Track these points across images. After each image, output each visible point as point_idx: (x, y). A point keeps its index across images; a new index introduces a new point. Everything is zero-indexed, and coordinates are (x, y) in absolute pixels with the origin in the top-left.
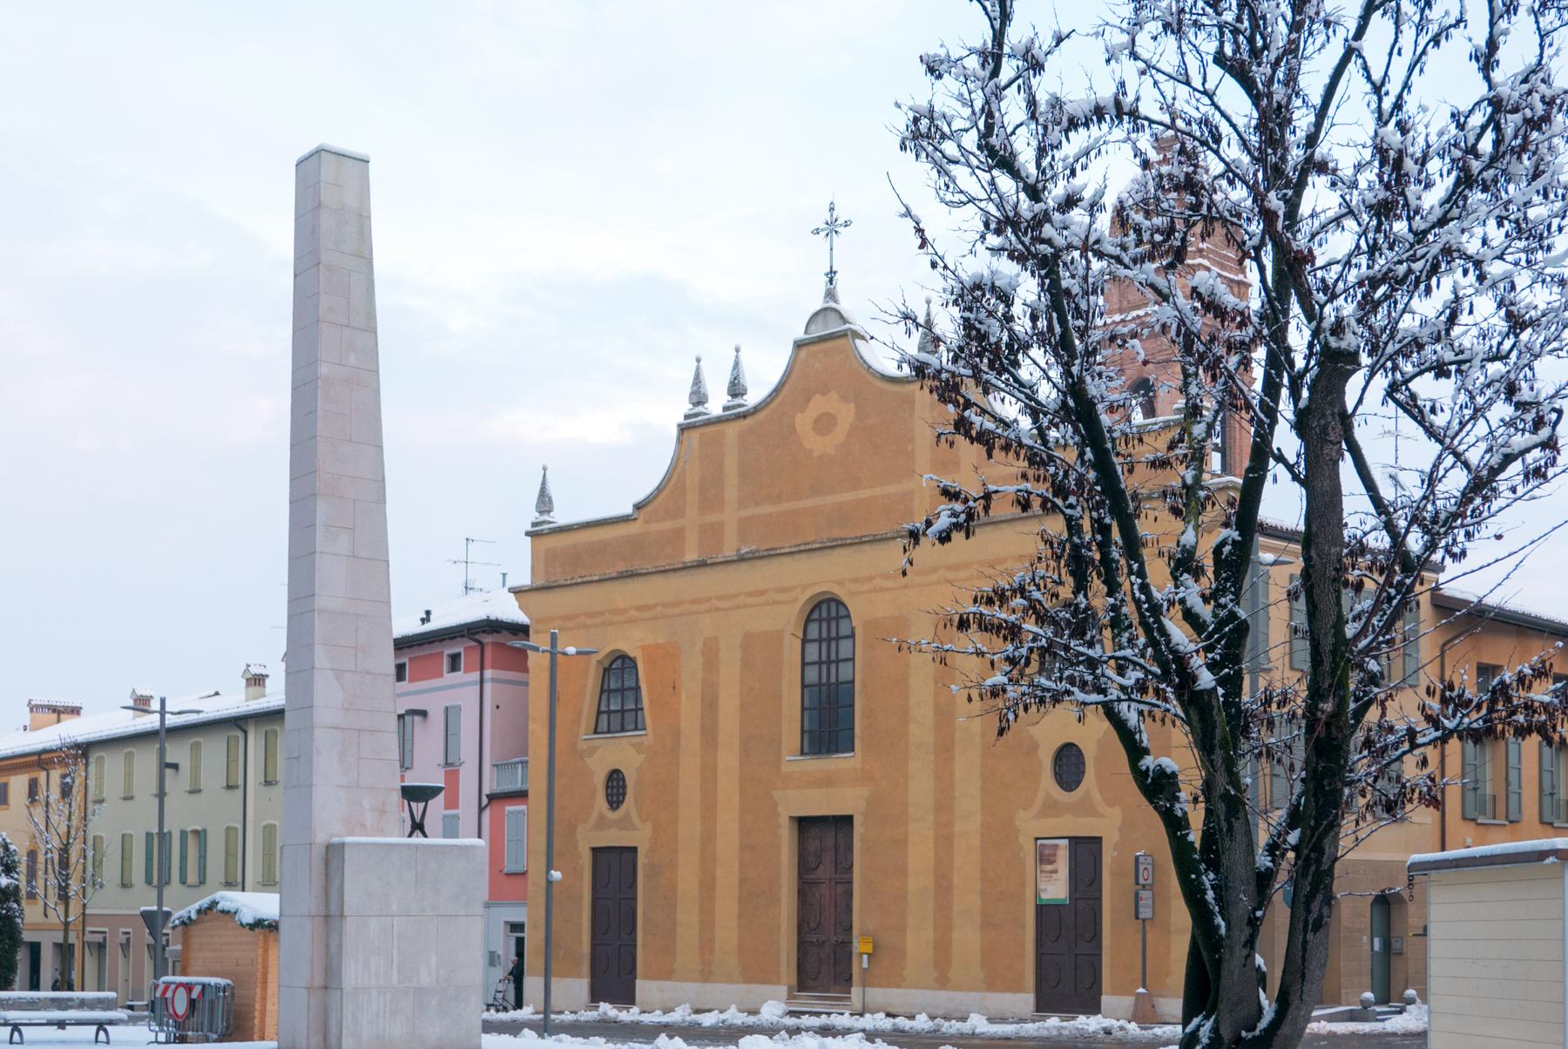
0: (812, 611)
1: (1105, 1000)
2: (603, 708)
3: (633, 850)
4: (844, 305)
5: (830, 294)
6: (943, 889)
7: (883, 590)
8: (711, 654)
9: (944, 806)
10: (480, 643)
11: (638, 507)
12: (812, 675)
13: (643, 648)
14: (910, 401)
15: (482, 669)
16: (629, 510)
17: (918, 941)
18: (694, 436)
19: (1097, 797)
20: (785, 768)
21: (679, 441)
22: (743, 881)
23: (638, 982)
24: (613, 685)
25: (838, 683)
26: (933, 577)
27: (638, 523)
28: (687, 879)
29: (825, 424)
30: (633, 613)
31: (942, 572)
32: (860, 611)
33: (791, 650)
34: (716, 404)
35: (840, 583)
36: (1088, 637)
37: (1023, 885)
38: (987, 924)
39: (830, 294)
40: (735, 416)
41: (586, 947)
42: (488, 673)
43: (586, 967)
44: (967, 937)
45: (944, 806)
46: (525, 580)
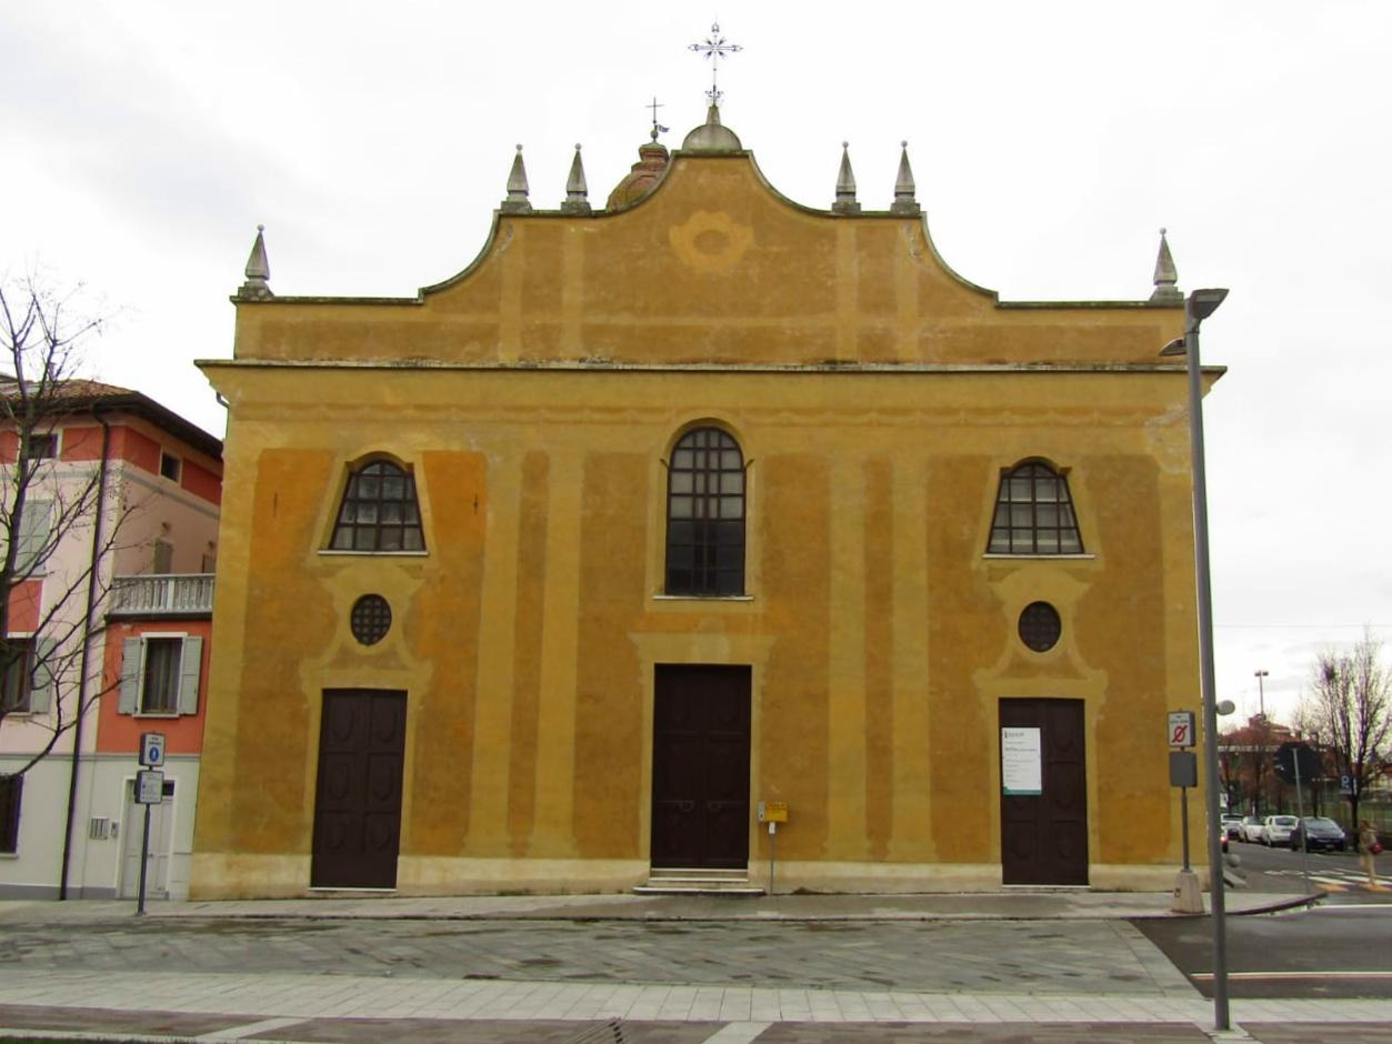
0: (683, 438)
1: (1095, 869)
2: (344, 520)
3: (400, 696)
4: (725, 120)
5: (714, 110)
6: (879, 749)
7: (792, 425)
8: (536, 472)
9: (878, 657)
10: (106, 426)
11: (427, 292)
12: (682, 508)
13: (426, 454)
14: (832, 237)
15: (105, 457)
16: (414, 295)
17: (490, 776)
18: (518, 227)
19: (1077, 659)
20: (648, 608)
21: (497, 228)
22: (581, 736)
23: (401, 859)
24: (363, 493)
25: (719, 519)
26: (864, 419)
27: (423, 311)
28: (490, 728)
29: (710, 241)
30: (411, 412)
31: (874, 416)
32: (756, 446)
33: (656, 475)
34: (547, 195)
35: (735, 412)
36: (40, 431)
37: (986, 747)
38: (939, 787)
39: (714, 110)
40: (576, 210)
41: (309, 816)
42: (116, 464)
43: (307, 841)
44: (555, 776)
45: (878, 657)
46: (225, 353)
